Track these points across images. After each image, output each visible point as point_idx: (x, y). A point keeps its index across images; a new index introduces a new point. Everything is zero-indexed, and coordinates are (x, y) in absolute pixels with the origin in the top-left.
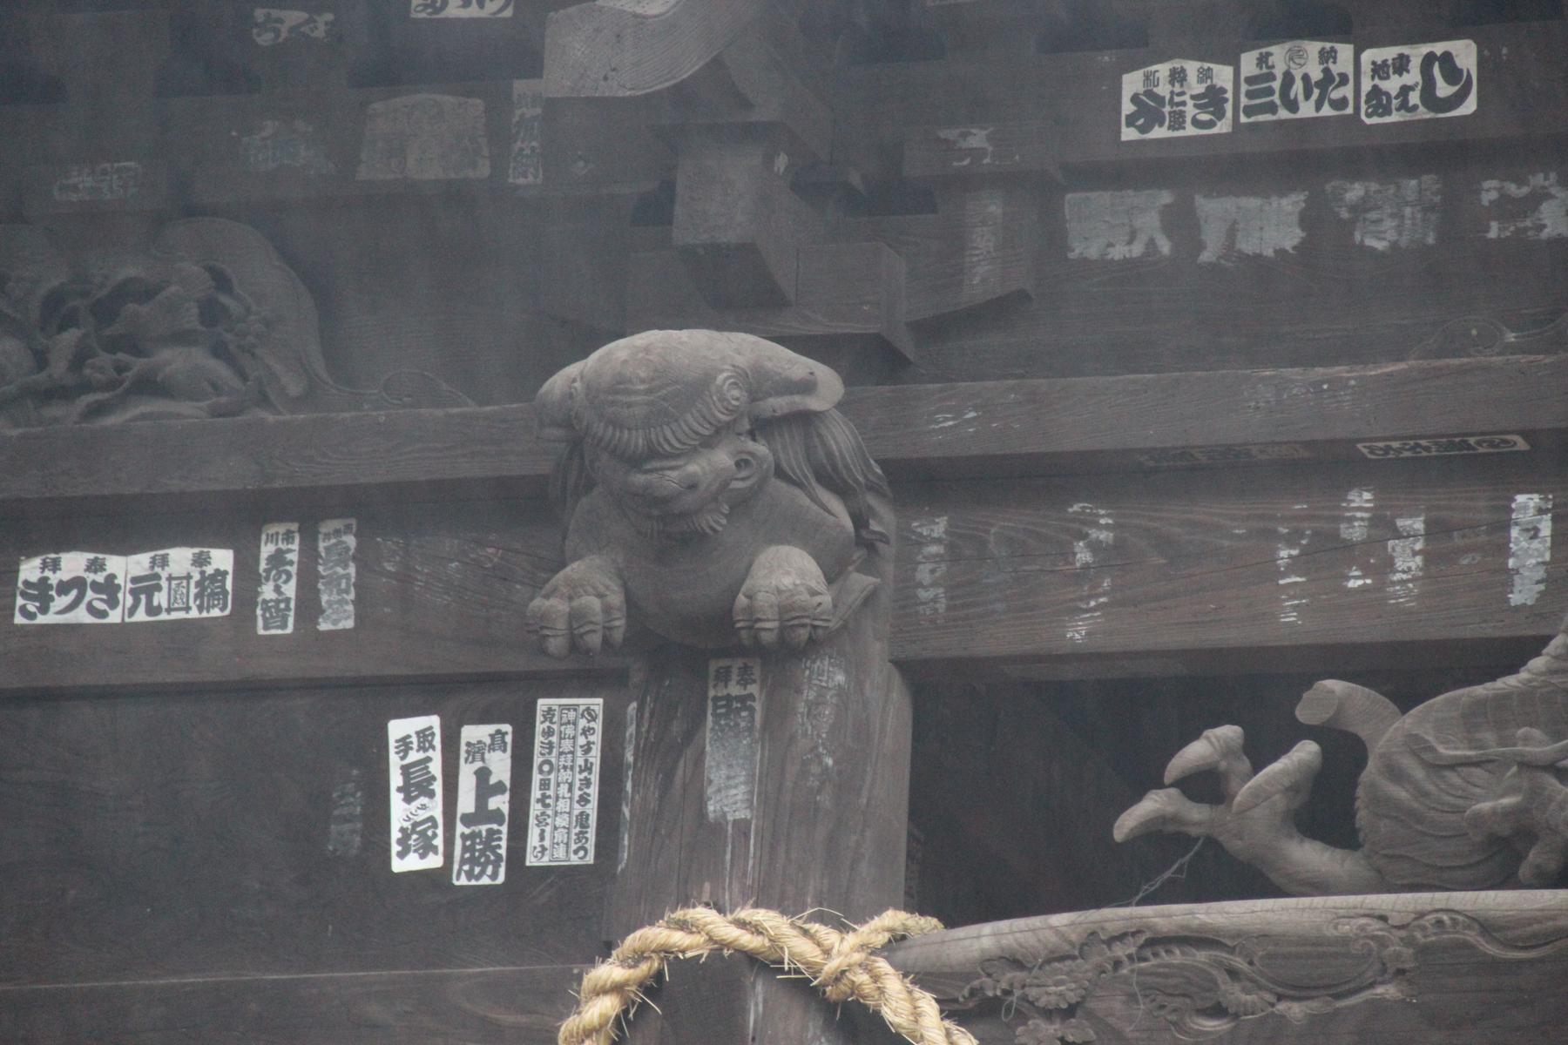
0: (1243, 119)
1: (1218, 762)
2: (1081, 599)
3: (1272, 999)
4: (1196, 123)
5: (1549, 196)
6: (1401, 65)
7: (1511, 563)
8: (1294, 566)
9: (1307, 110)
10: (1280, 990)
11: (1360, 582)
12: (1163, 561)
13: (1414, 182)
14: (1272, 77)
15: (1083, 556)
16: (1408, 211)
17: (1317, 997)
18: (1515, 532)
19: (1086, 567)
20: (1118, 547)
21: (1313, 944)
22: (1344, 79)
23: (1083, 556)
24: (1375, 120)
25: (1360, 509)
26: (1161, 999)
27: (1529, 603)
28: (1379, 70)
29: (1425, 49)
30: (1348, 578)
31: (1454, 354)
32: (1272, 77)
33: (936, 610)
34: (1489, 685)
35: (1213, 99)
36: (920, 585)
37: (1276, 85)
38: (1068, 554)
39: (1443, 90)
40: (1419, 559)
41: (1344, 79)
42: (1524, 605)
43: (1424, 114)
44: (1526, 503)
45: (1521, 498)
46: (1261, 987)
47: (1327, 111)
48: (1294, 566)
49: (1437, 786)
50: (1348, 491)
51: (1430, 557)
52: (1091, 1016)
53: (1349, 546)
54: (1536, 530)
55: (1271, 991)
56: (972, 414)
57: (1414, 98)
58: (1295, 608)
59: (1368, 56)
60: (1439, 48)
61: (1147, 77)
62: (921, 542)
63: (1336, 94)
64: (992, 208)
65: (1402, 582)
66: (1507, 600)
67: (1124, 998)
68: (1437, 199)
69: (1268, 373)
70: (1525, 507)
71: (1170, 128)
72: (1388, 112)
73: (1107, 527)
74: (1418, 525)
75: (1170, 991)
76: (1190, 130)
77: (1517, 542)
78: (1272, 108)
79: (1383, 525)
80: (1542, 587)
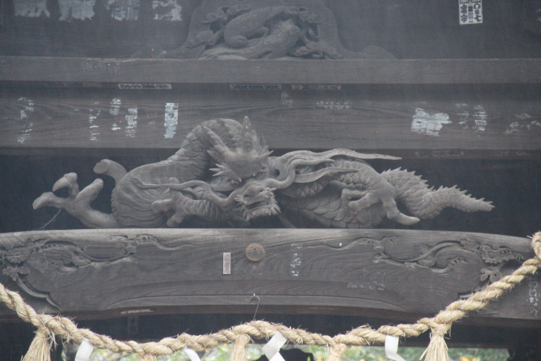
3: (89, 261)
8: (94, 122)
10: (92, 258)
15: (23, 115)
16: (129, 9)
18: (166, 115)
19: (24, 119)
26: (53, 261)
27: (171, 137)
30: (113, 127)
40: (136, 122)
44: (170, 106)
48: (94, 122)
52: (29, 265)
55: (89, 259)
58: (95, 136)
65: (130, 129)
68: (138, 5)
69: (96, 103)
73: (31, 106)
74: (135, 111)
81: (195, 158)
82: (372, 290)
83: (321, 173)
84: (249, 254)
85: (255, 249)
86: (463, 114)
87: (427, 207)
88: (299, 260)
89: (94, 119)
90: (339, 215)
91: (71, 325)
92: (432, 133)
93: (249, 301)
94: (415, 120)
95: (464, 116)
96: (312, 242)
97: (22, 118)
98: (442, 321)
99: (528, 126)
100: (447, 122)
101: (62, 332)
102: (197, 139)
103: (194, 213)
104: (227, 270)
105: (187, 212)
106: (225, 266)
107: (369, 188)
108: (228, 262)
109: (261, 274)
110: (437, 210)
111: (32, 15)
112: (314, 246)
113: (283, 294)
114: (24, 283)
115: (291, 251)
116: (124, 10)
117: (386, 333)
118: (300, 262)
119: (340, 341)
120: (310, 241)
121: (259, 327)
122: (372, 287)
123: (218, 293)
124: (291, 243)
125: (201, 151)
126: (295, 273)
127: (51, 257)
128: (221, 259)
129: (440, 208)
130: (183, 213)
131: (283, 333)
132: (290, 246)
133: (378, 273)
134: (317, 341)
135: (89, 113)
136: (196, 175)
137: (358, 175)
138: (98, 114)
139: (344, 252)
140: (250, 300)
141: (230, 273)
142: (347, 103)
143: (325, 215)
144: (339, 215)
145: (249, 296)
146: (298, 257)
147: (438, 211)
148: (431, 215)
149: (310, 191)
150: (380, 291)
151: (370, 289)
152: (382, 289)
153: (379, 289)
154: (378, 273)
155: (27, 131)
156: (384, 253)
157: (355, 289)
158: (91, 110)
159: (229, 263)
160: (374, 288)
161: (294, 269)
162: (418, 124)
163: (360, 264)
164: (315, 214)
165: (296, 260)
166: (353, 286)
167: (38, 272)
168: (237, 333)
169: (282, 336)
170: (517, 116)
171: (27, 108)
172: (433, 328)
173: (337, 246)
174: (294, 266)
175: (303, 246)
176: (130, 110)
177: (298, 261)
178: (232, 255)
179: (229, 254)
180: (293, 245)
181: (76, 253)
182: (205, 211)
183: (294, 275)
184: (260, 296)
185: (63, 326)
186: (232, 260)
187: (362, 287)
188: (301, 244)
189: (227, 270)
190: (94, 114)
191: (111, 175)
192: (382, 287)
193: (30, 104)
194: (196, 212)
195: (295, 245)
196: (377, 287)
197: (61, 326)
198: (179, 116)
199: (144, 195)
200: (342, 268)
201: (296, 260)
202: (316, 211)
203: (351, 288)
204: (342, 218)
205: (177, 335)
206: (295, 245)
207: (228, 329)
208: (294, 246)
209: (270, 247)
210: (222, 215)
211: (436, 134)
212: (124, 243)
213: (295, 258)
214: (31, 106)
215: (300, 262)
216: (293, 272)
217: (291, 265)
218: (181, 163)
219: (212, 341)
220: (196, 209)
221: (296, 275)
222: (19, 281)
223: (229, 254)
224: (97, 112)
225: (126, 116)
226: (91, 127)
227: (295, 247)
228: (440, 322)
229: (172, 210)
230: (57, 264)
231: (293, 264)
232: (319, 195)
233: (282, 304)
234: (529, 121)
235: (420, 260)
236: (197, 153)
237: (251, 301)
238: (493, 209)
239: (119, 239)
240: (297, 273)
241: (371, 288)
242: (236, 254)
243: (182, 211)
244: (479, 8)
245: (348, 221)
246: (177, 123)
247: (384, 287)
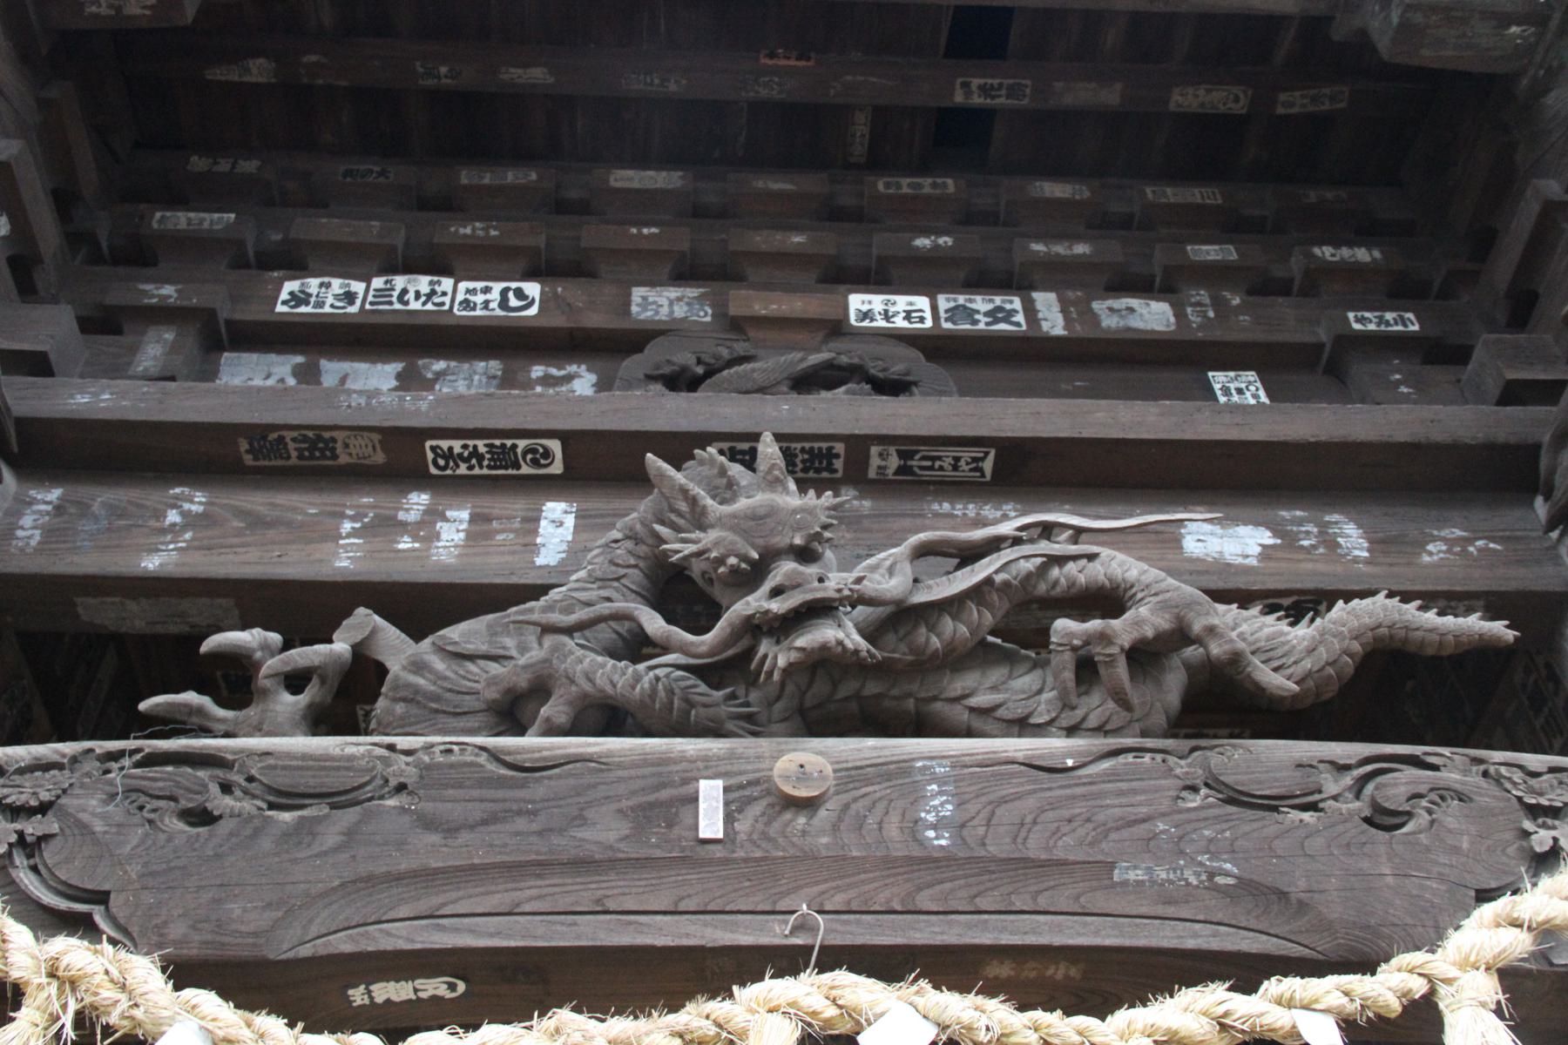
0: (368, 307)
1: (254, 651)
2: (162, 543)
3: (265, 806)
4: (332, 306)
5: (580, 376)
6: (487, 290)
7: (539, 540)
8: (354, 533)
9: (415, 305)
10: (271, 798)
11: (410, 545)
12: (242, 525)
13: (483, 364)
14: (393, 290)
15: (173, 517)
16: (476, 378)
17: (311, 805)
18: (543, 523)
19: (174, 525)
20: (204, 516)
21: (315, 760)
22: (444, 294)
23: (173, 517)
24: (464, 313)
25: (418, 504)
26: (143, 799)
27: (552, 564)
28: (468, 291)
29: (504, 285)
30: (399, 542)
31: (500, 467)
32: (393, 290)
33: (28, 544)
34: (492, 791)
35: (350, 297)
36: (22, 528)
37: (396, 294)
38: (160, 515)
39: (514, 302)
40: (462, 535)
41: (444, 294)
42: (548, 566)
43: (499, 312)
44: (555, 509)
45: (550, 505)
46: (254, 797)
47: (430, 307)
48: (354, 533)
49: (456, 673)
50: (410, 491)
51: (470, 536)
52: (64, 815)
53: (404, 524)
54: (561, 524)
55: (264, 800)
56: (107, 397)
57: (493, 305)
58: (349, 558)
59: (463, 286)
60: (514, 285)
61: (303, 284)
62: (33, 501)
63: (437, 300)
64: (167, 336)
65: (445, 547)
66: (534, 562)
67: (104, 797)
68: (500, 373)
69: (365, 500)
70: (554, 510)
71: (314, 307)
72: (474, 309)
73: (200, 503)
74: (465, 515)
75: (157, 793)
76: (327, 309)
77: (545, 528)
78: (391, 303)
79: (434, 514)
80: (564, 555)
81: (616, 584)
82: (1197, 887)
83: (990, 564)
84: (786, 778)
85: (802, 766)
86: (1303, 529)
87: (1314, 650)
88: (947, 802)
89: (353, 528)
90: (1043, 707)
91: (145, 972)
92: (1240, 560)
93: (787, 932)
94: (1188, 538)
95: (1308, 533)
96: (980, 757)
97: (167, 523)
98: (1472, 959)
99: (1471, 549)
100: (1271, 541)
101: (108, 993)
102: (627, 537)
103: (609, 689)
104: (711, 824)
105: (587, 687)
106: (705, 815)
107: (1140, 596)
108: (715, 804)
109: (824, 840)
110: (1346, 652)
111: (258, 382)
112: (987, 766)
113: (899, 908)
114: (35, 869)
115: (916, 779)
116: (465, 379)
117: (1292, 998)
118: (950, 807)
119: (1132, 1028)
120: (973, 755)
121: (832, 988)
122: (1197, 874)
123: (682, 907)
124: (913, 760)
125: (635, 566)
126: (937, 838)
127: (143, 792)
128: (694, 799)
129: (1356, 647)
130: (574, 688)
131: (920, 1008)
132: (913, 767)
133: (1207, 833)
134: (1048, 1034)
135: (343, 516)
136: (617, 633)
137: (1102, 565)
138: (366, 520)
139: (1085, 780)
140: (789, 927)
141: (720, 835)
142: (1010, 507)
143: (1001, 713)
144: (1043, 707)
145: (787, 917)
146: (941, 793)
147: (1351, 655)
148: (1330, 671)
149: (955, 631)
150: (1217, 889)
151: (1188, 884)
152: (1231, 881)
153: (1220, 880)
154: (1207, 833)
155: (171, 546)
156: (1207, 785)
157: (1139, 883)
158: (350, 512)
159: (717, 808)
160: (1204, 877)
161: (934, 827)
162: (1200, 544)
163: (1144, 810)
164: (972, 710)
165: (936, 802)
166: (1132, 876)
167: (85, 829)
168: (755, 1006)
169: (921, 1017)
170: (1436, 533)
171: (186, 506)
172: (1448, 981)
173: (1060, 766)
174: (931, 818)
175: (953, 767)
176: (449, 514)
177: (942, 804)
178: (726, 790)
179: (719, 783)
180: (920, 764)
181: (226, 788)
182: (642, 688)
183: (936, 842)
184: (826, 916)
185: (115, 973)
186: (727, 804)
187: (1164, 875)
188: (944, 762)
189: (711, 824)
190: (353, 519)
191: (380, 658)
192: (1227, 874)
193: (196, 499)
194: (614, 686)
195: (928, 763)
196: (1212, 875)
197: (107, 972)
198: (575, 527)
199: (462, 672)
200: (1088, 820)
201: (936, 802)
202: (973, 701)
203: (1125, 883)
204: (1054, 715)
205: (531, 1018)
206: (928, 763)
207: (1067, 244)
208: (924, 766)
209: (847, 769)
210: (693, 712)
211: (1253, 562)
212: (379, 758)
213: (933, 796)
214: (200, 503)
215: (950, 807)
216: (931, 834)
217: (923, 815)
218: (575, 594)
219: (662, 1035)
220: (616, 678)
221: (943, 842)
222: (18, 862)
223: (719, 783)
224: (366, 516)
225: (439, 525)
226: (341, 542)
227: (925, 768)
228: (1467, 965)
229: (540, 690)
230: (154, 811)
231: (928, 812)
232: (978, 654)
233: (899, 941)
234: (1470, 541)
235: (1323, 800)
236: (622, 571)
237: (791, 933)
238: (1516, 638)
239: (369, 752)
240: (943, 837)
241: (1193, 880)
242: (741, 787)
243: (572, 682)
244: (1257, 389)
245: (1072, 722)
246: (570, 538)
247: (1235, 871)
